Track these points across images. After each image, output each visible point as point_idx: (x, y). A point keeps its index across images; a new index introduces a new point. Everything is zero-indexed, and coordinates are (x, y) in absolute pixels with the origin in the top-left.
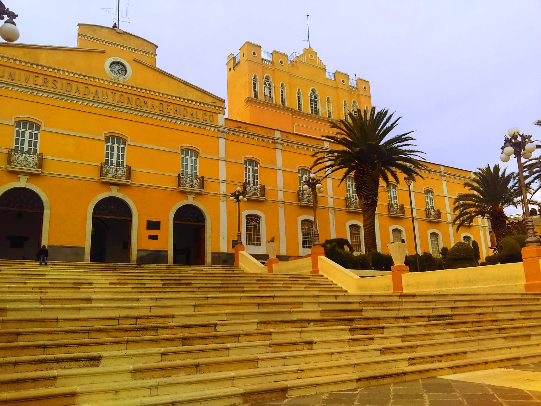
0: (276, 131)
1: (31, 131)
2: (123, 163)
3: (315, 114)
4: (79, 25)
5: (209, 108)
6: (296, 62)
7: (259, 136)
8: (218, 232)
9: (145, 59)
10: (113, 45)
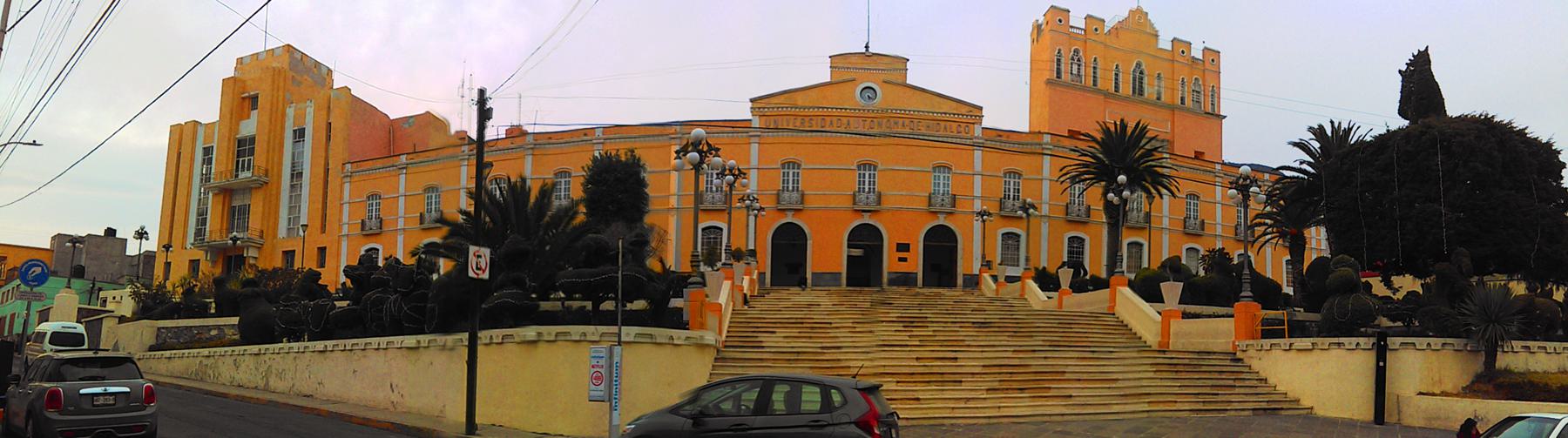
0: (1045, 135)
4: (830, 57)
6: (1116, 29)
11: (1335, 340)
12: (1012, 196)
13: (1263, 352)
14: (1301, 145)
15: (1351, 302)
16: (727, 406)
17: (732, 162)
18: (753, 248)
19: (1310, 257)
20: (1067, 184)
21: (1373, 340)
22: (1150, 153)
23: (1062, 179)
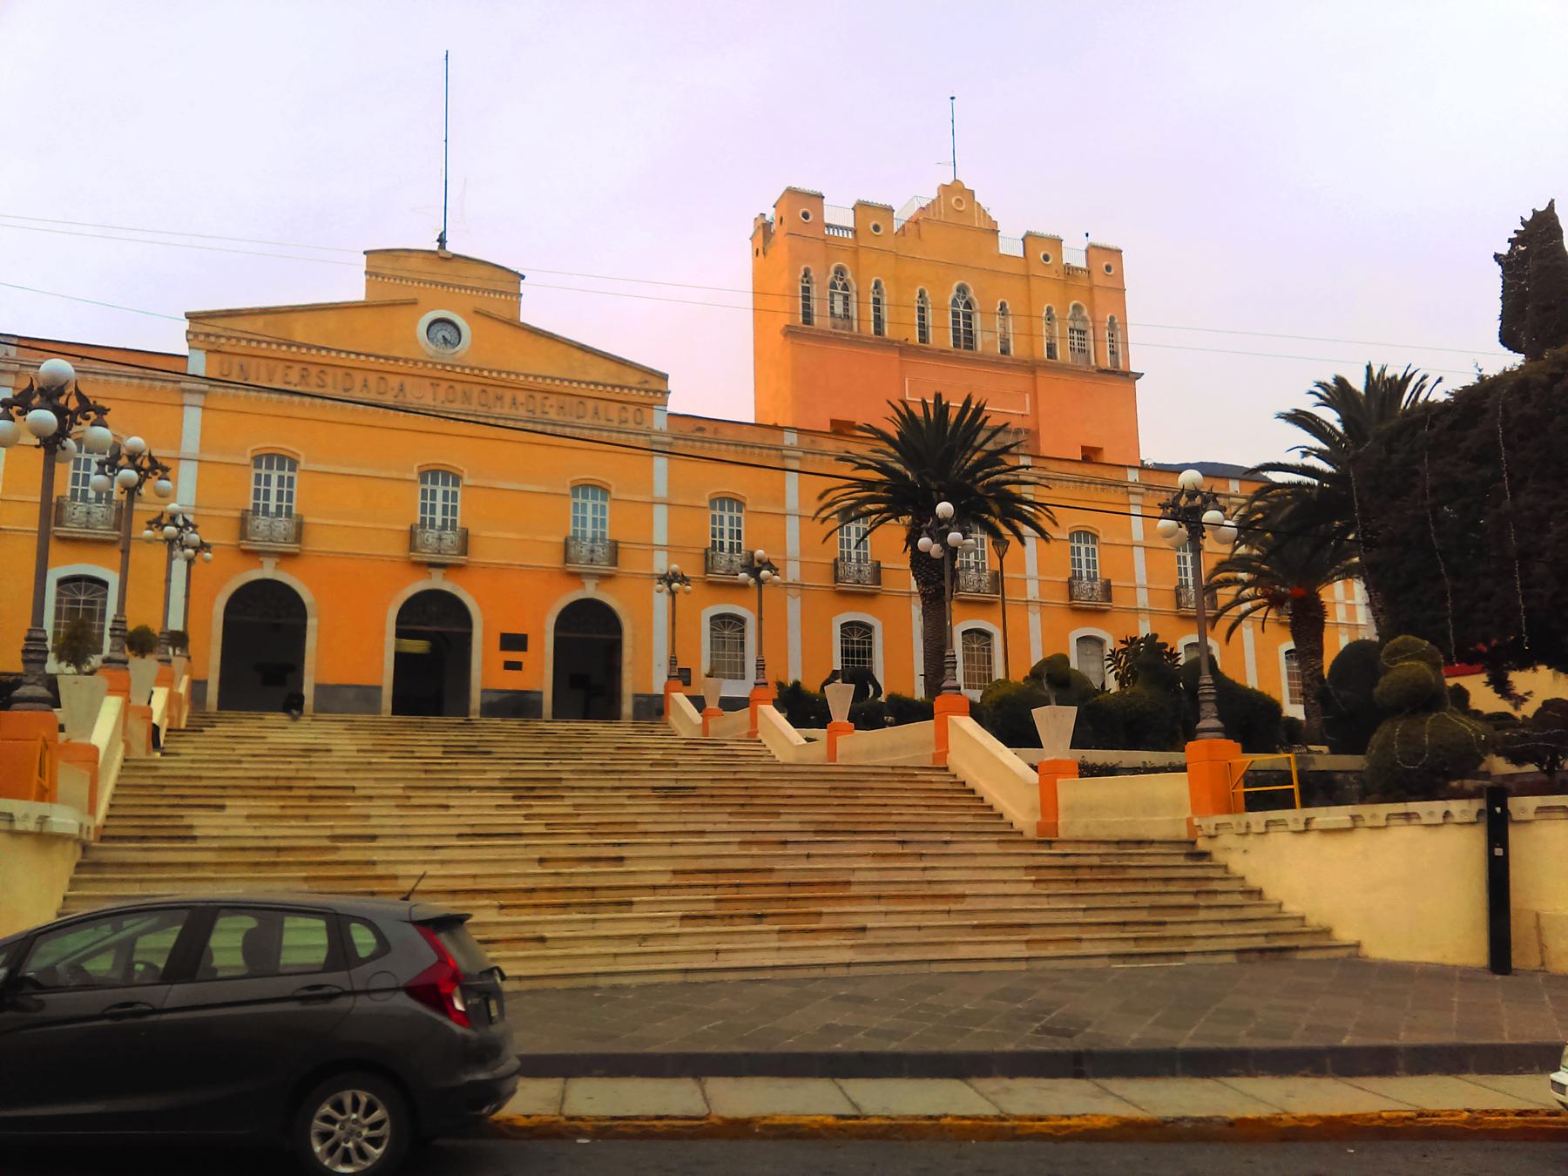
1: (281, 473)
2: (454, 522)
3: (966, 347)
5: (635, 396)
6: (916, 223)
7: (744, 446)
8: (649, 653)
9: (496, 305)
10: (433, 286)
11: (1400, 808)
12: (727, 545)
13: (1251, 838)
14: (1301, 419)
15: (1428, 728)
16: (101, 966)
17: (135, 441)
18: (180, 627)
19: (1336, 642)
20: (835, 522)
21: (1477, 805)
22: (993, 458)
23: (824, 514)
